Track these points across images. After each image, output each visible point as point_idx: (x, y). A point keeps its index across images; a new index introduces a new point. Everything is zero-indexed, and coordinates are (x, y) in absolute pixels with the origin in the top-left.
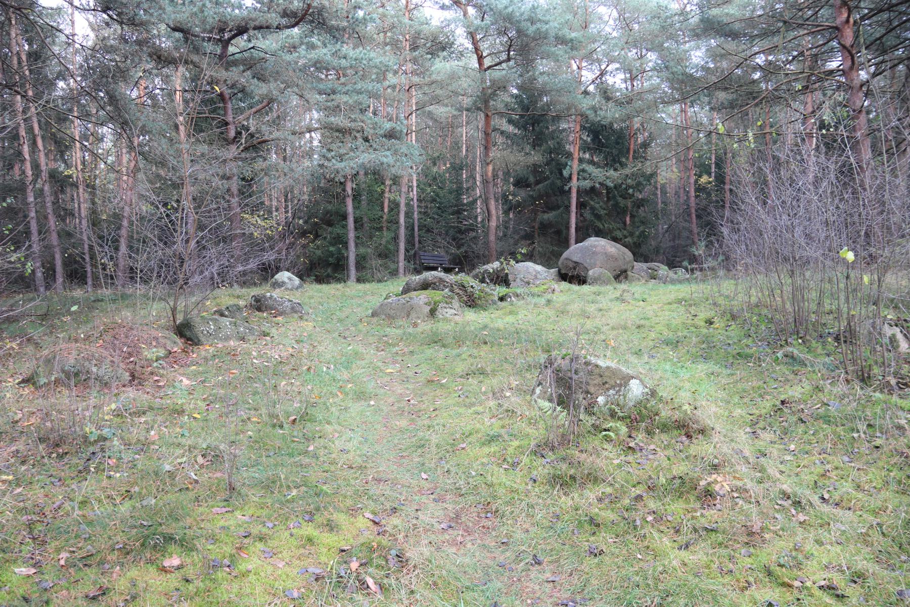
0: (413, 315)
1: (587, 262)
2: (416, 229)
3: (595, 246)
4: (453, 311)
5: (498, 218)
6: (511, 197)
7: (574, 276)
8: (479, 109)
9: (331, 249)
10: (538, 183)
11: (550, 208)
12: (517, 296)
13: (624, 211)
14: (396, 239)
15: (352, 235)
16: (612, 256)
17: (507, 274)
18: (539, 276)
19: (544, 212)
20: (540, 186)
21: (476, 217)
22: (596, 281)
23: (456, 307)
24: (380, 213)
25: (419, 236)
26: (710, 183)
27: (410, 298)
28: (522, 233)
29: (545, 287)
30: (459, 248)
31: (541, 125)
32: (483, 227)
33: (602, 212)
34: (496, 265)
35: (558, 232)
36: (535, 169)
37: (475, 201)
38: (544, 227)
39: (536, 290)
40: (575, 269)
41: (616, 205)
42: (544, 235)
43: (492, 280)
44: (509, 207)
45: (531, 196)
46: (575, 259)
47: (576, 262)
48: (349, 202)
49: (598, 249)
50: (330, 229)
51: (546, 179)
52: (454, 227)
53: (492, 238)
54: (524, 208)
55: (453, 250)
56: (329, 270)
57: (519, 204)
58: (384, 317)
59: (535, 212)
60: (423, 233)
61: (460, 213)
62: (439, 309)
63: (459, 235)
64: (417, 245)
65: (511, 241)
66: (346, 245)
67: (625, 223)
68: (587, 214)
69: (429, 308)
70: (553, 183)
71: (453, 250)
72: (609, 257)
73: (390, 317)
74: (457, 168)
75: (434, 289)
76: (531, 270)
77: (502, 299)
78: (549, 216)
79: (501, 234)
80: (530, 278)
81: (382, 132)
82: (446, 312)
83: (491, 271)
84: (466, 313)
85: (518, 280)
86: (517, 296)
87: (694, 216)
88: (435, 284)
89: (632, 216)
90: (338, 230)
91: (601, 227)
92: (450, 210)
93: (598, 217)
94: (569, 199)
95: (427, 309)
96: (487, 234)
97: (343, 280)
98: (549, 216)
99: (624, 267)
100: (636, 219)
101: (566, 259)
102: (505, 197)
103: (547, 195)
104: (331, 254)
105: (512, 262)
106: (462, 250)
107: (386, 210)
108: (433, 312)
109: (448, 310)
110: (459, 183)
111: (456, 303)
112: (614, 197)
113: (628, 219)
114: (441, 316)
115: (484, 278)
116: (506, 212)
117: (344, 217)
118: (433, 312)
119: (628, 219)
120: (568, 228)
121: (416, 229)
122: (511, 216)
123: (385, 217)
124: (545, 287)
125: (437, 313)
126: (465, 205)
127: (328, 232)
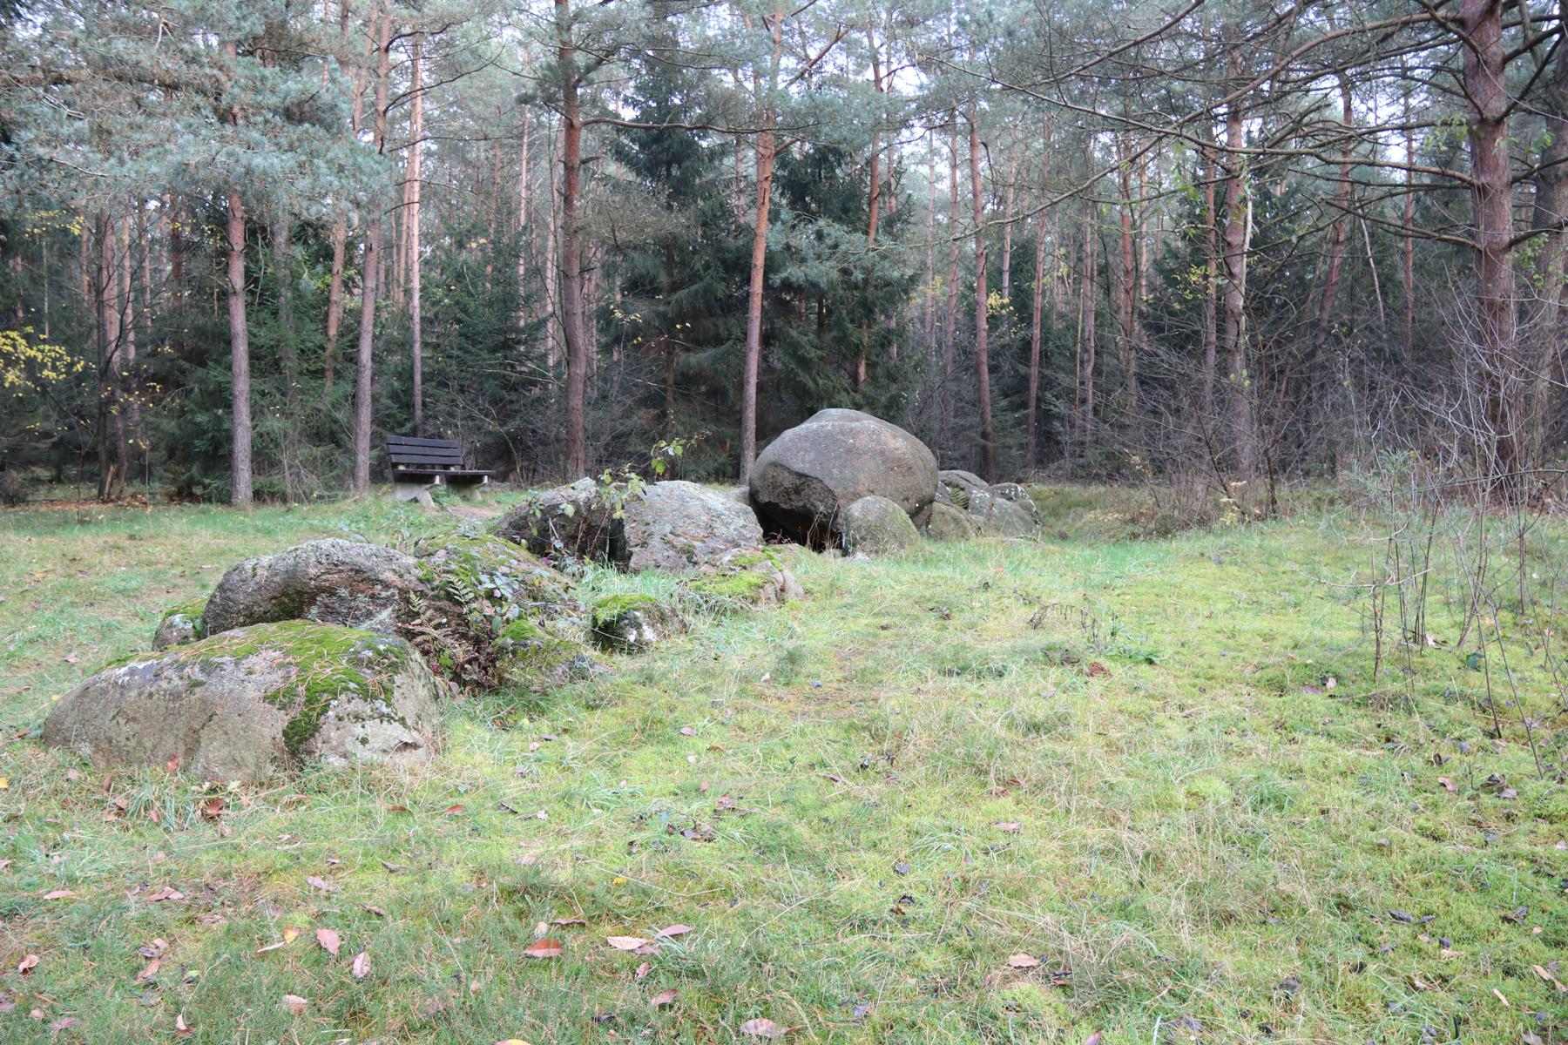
0: (213, 750)
1: (833, 475)
2: (418, 378)
3: (853, 433)
4: (396, 733)
5: (589, 361)
6: (618, 315)
7: (793, 519)
8: (549, 100)
9: (199, 418)
10: (675, 287)
11: (698, 341)
12: (663, 619)
13: (857, 350)
14: (354, 399)
15: (242, 386)
16: (899, 462)
17: (620, 523)
18: (720, 530)
19: (688, 350)
20: (682, 294)
21: (543, 357)
22: (874, 539)
23: (407, 708)
24: (319, 338)
25: (424, 394)
26: (1003, 306)
27: (208, 667)
28: (640, 393)
29: (752, 577)
30: (503, 423)
31: (687, 163)
32: (558, 377)
33: (813, 354)
34: (584, 488)
35: (717, 393)
36: (669, 248)
37: (542, 323)
38: (687, 381)
39: (722, 590)
40: (797, 491)
41: (842, 340)
42: (686, 397)
43: (570, 539)
44: (616, 337)
45: (662, 316)
46: (798, 466)
47: (800, 475)
48: (238, 308)
49: (863, 442)
50: (200, 372)
51: (695, 277)
52: (494, 376)
53: (577, 402)
54: (647, 339)
55: (492, 426)
56: (195, 470)
57: (636, 329)
58: (86, 749)
59: (670, 348)
60: (430, 387)
61: (511, 348)
62: (329, 730)
63: (510, 392)
64: (419, 413)
65: (617, 410)
66: (229, 405)
67: (854, 377)
68: (778, 360)
69: (281, 720)
70: (708, 290)
71: (492, 426)
72: (893, 464)
73: (110, 750)
74: (504, 254)
75: (329, 613)
76: (694, 508)
77: (608, 635)
78: (700, 358)
79: (595, 394)
80: (691, 534)
81: (274, 100)
82: (359, 739)
83: (570, 510)
84: (461, 729)
85: (655, 542)
86: (663, 619)
87: (985, 369)
88: (331, 592)
89: (871, 366)
90: (215, 373)
91: (811, 384)
92: (489, 342)
93: (804, 362)
94: (745, 322)
95: (274, 724)
96: (565, 392)
97: (225, 498)
98: (700, 358)
99: (928, 491)
100: (879, 371)
101: (775, 465)
102: (605, 315)
103: (695, 316)
104: (200, 432)
105: (636, 484)
106: (511, 426)
107: (333, 332)
108: (298, 742)
109: (372, 727)
110: (510, 282)
111: (413, 687)
112: (839, 324)
113: (862, 370)
114: (336, 762)
115: (545, 532)
116: (606, 349)
117: (227, 341)
118: (298, 742)
119: (862, 370)
120: (741, 386)
121: (418, 378)
122: (616, 357)
123: (330, 347)
124: (752, 577)
125: (318, 744)
126: (522, 331)
127: (197, 378)
